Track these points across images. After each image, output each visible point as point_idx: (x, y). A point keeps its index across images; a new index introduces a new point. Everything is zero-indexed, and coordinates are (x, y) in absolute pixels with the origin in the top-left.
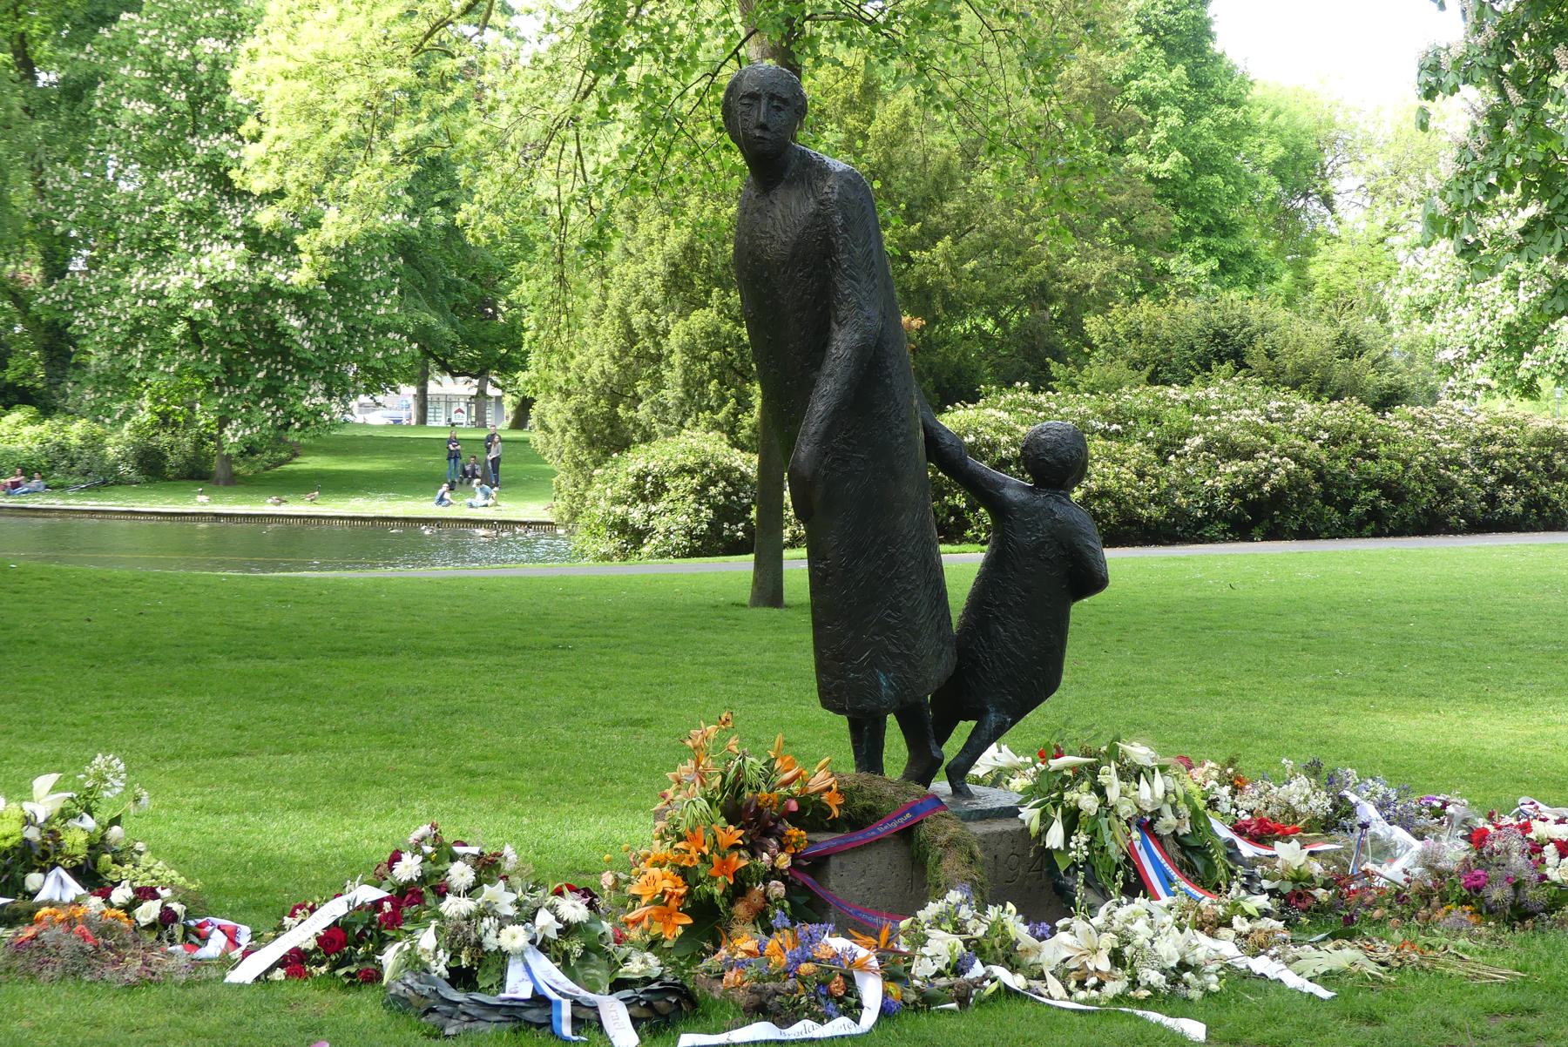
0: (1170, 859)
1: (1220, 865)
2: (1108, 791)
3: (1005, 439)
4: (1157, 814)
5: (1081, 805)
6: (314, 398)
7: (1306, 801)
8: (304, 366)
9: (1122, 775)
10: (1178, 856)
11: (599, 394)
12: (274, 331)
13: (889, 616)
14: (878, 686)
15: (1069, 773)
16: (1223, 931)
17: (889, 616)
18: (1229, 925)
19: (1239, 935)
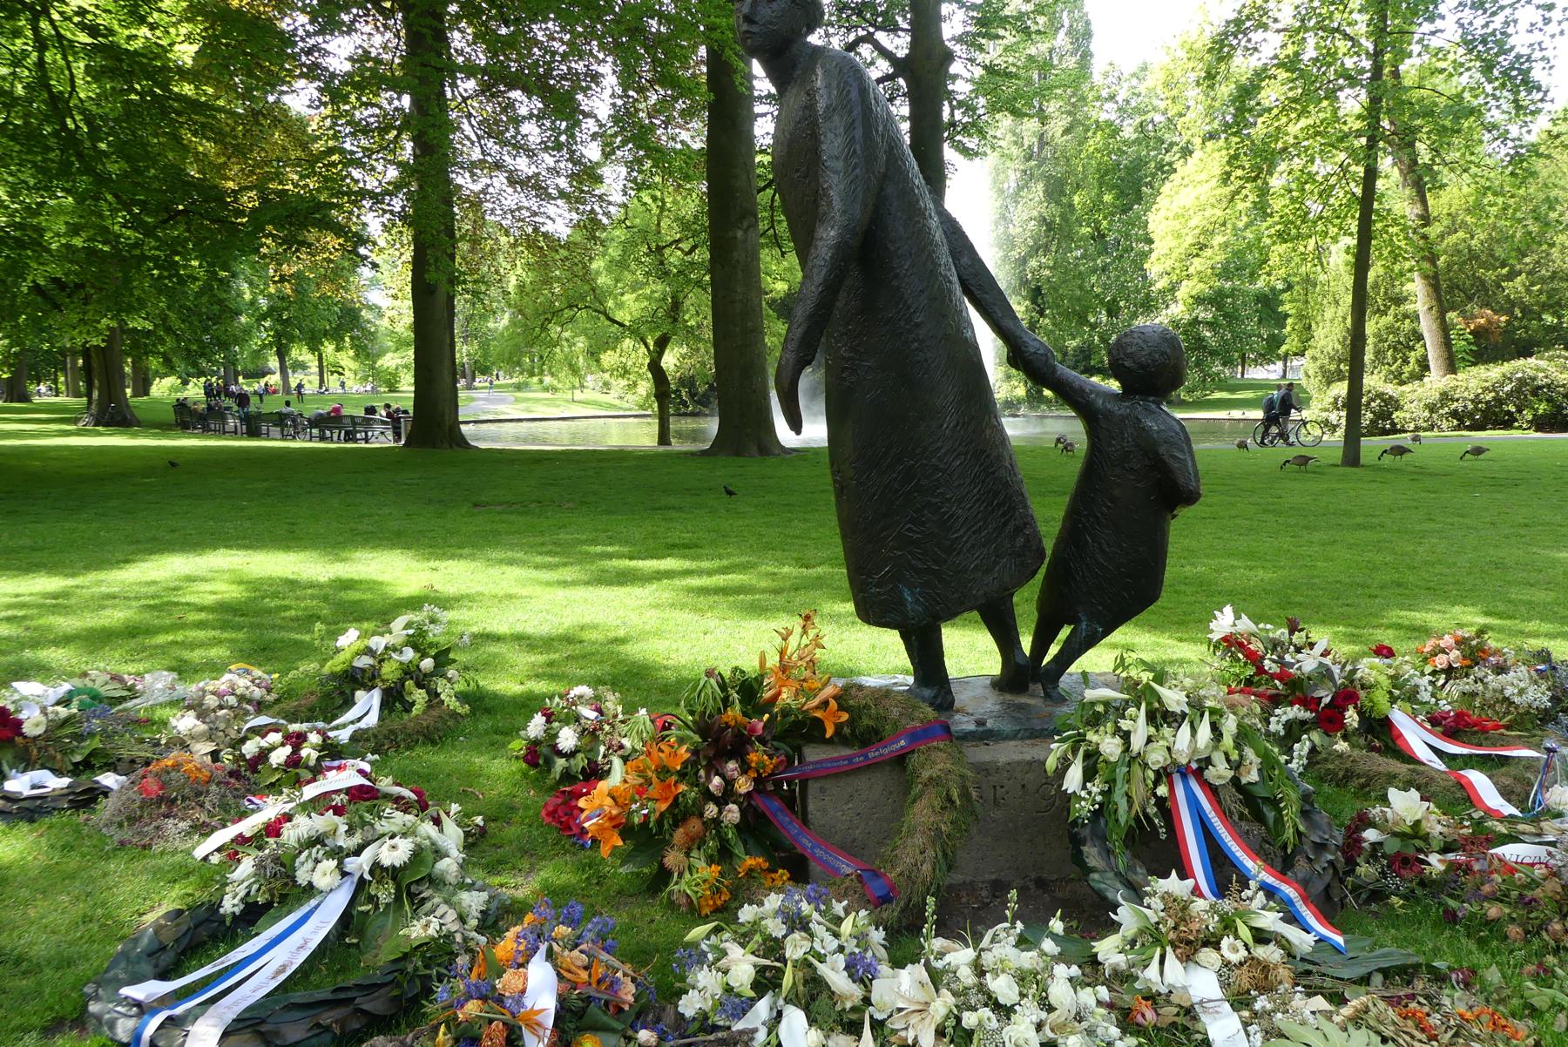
0: (1225, 814)
1: (1289, 824)
2: (1132, 738)
3: (1541, 375)
4: (1208, 761)
5: (1101, 749)
6: (1217, 368)
7: (1521, 692)
8: (1213, 353)
9: (1151, 718)
10: (1236, 807)
11: (1332, 359)
12: (1200, 339)
13: (909, 530)
14: (902, 601)
15: (1100, 708)
16: (1207, 955)
17: (909, 530)
18: (1217, 946)
19: (1227, 964)
